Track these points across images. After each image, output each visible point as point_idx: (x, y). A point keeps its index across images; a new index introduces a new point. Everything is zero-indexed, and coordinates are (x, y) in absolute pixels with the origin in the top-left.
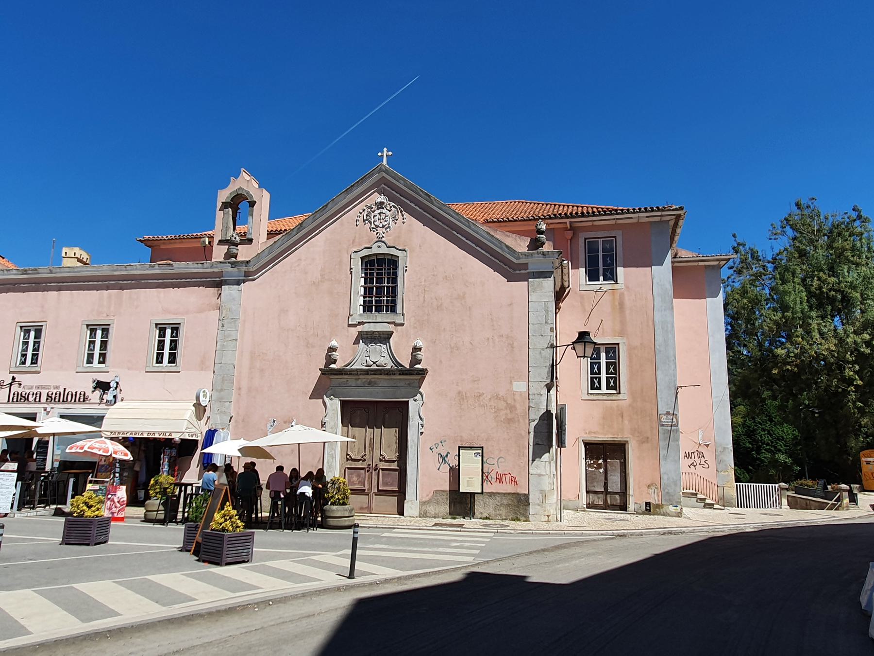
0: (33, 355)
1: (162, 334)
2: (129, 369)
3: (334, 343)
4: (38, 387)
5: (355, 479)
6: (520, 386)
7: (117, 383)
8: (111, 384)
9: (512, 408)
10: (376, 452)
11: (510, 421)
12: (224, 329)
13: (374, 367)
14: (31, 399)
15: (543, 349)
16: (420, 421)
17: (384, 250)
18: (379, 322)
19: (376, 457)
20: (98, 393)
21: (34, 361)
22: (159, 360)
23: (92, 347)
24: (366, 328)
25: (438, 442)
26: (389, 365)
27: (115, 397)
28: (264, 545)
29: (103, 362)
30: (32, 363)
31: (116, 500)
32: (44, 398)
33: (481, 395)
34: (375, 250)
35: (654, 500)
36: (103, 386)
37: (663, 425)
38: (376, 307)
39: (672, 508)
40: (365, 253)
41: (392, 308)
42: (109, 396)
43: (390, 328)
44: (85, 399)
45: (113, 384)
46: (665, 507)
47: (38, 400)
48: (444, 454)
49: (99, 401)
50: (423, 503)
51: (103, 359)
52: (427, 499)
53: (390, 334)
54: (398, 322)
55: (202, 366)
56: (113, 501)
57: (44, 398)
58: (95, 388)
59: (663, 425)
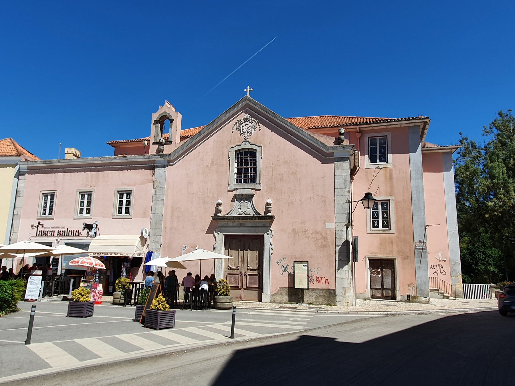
1: (121, 197)
2: (103, 217)
3: (220, 201)
4: (53, 228)
5: (233, 280)
7: (97, 225)
8: (93, 226)
9: (325, 239)
10: (245, 265)
13: (243, 215)
14: (49, 234)
15: (343, 203)
17: (248, 146)
18: (246, 189)
19: (245, 267)
20: (86, 231)
22: (120, 211)
24: (238, 192)
25: (282, 258)
26: (252, 214)
27: (95, 233)
29: (89, 213)
31: (97, 292)
34: (243, 146)
35: (412, 293)
36: (89, 227)
37: (417, 249)
38: (244, 180)
39: (423, 299)
40: (237, 148)
41: (254, 180)
42: (92, 233)
44: (79, 234)
45: (94, 226)
46: (419, 298)
48: (285, 266)
49: (86, 236)
50: (273, 295)
51: (88, 211)
52: (275, 292)
53: (252, 196)
54: (257, 188)
55: (144, 215)
56: (95, 292)
58: (84, 228)
59: (417, 249)
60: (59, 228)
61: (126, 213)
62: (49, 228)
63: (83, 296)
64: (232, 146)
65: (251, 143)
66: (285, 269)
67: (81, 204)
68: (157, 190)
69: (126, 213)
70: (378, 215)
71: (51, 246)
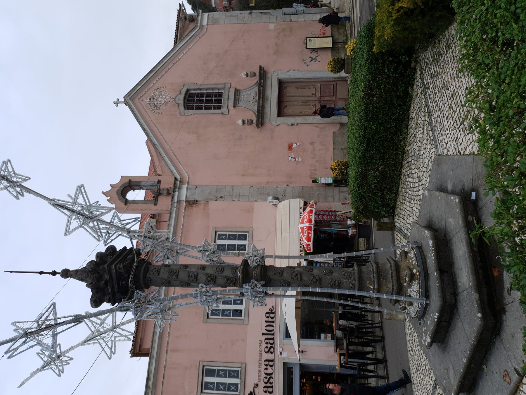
0: (229, 239)
3: (240, 122)
4: (260, 364)
6: (272, 26)
9: (284, 30)
10: (310, 99)
11: (291, 30)
12: (223, 196)
14: (270, 371)
16: (291, 71)
17: (182, 97)
18: (228, 99)
21: (233, 374)
23: (227, 313)
24: (231, 103)
25: (303, 62)
26: (256, 89)
28: (327, 43)
30: (237, 377)
32: (269, 356)
33: (276, 43)
34: (181, 102)
38: (219, 97)
40: (182, 107)
43: (232, 91)
47: (270, 363)
48: (311, 59)
55: (250, 211)
57: (269, 356)
60: (260, 352)
61: (245, 239)
62: (260, 371)
63: (356, 160)
64: (178, 113)
65: (178, 93)
66: (314, 59)
67: (226, 315)
68: (219, 196)
69: (245, 239)
70: (222, 239)
71: (280, 113)
